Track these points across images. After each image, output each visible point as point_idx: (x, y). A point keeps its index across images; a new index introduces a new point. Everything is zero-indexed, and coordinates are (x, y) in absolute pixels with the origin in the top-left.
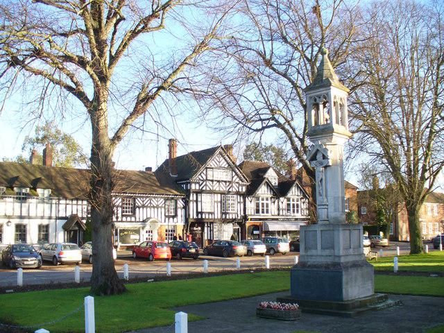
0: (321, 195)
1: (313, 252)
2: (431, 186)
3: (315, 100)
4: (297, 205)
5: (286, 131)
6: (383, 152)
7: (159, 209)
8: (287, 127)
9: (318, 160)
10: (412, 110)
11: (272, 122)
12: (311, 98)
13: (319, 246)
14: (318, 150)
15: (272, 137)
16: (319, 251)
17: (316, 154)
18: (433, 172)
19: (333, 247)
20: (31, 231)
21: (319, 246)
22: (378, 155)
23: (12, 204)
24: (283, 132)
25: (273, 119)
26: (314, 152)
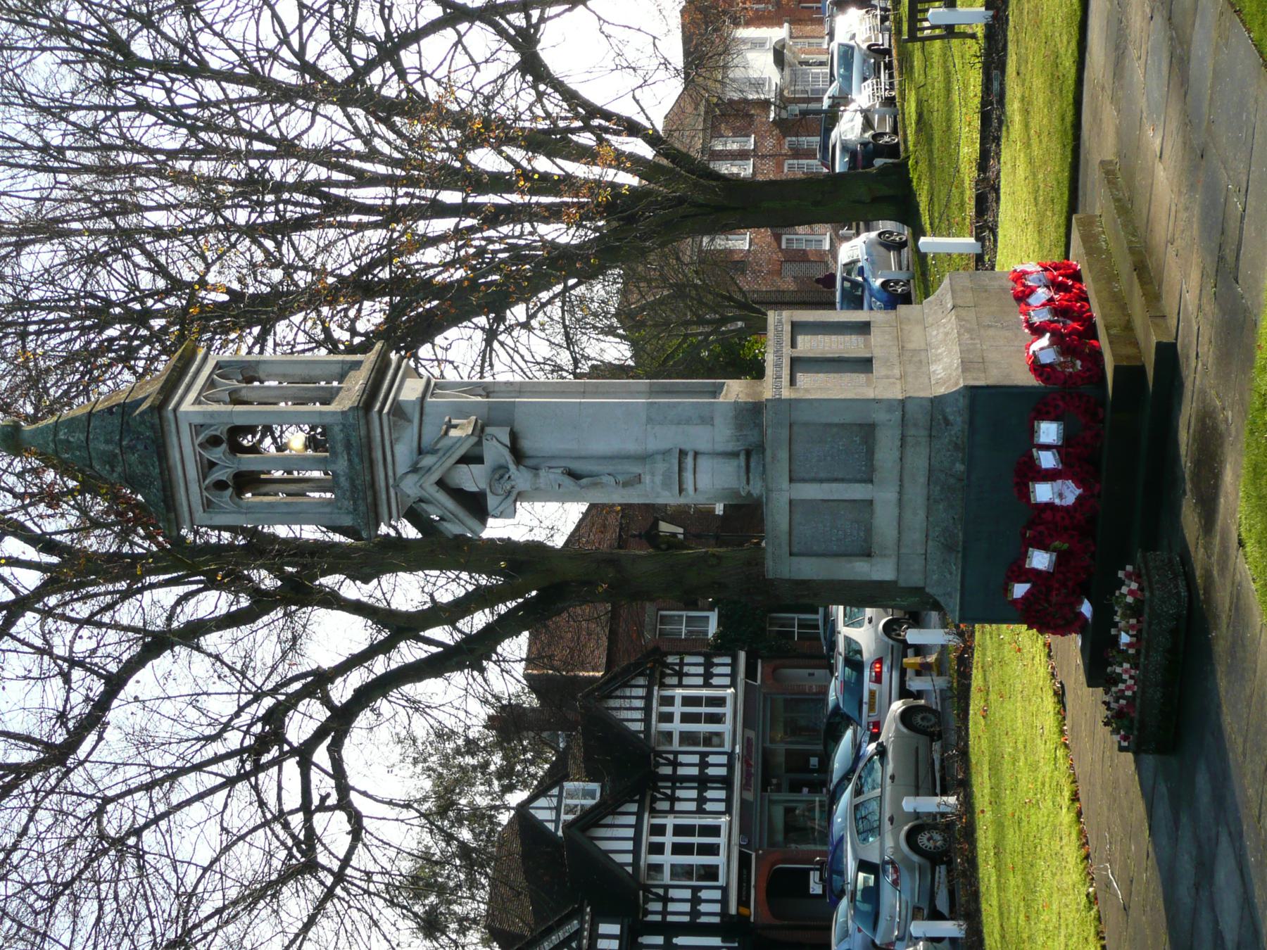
0: (638, 479)
1: (885, 521)
2: (632, 129)
3: (220, 485)
4: (679, 830)
5: (365, 696)
6: (482, 321)
7: (686, 669)
8: (341, 691)
9: (483, 485)
10: (313, 188)
11: (321, 755)
12: (208, 505)
13: (858, 492)
14: (441, 483)
15: (383, 760)
16: (884, 496)
17: (458, 494)
18: (577, 117)
19: (867, 432)
20: (1264, 931)
21: (858, 492)
22: (491, 335)
23: (277, 40)
24: (364, 718)
25: (304, 754)
26: (449, 503)
